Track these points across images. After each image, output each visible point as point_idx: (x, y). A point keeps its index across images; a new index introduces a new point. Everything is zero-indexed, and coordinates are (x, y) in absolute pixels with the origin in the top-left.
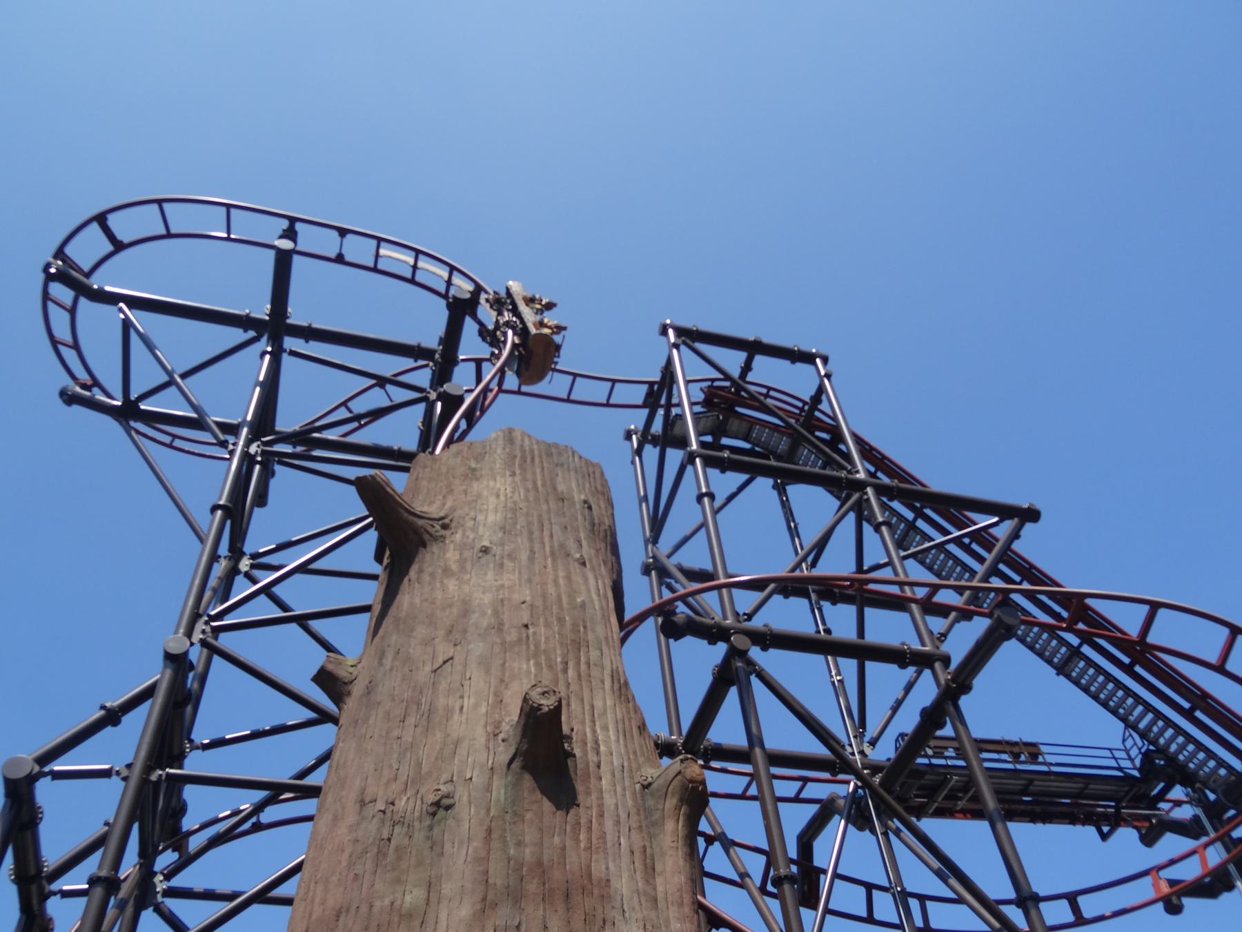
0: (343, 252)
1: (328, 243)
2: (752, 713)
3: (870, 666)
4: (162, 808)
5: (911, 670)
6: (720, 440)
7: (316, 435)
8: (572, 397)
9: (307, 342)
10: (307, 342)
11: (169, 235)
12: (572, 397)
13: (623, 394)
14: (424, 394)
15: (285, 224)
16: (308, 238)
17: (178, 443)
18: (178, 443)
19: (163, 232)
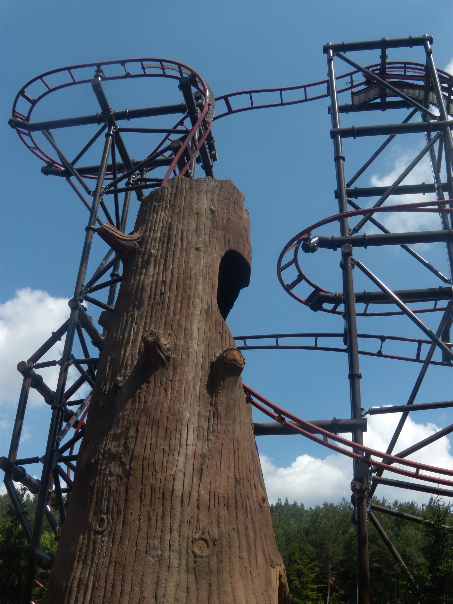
0: (123, 67)
1: (119, 70)
2: (124, 225)
3: (246, 340)
4: (209, 95)
5: (345, 347)
6: (385, 100)
7: (160, 157)
8: (308, 98)
9: (366, 247)
10: (366, 247)
11: (50, 91)
12: (303, 89)
13: (312, 92)
14: (349, 199)
15: (95, 68)
16: (108, 71)
17: (413, 470)
18: (413, 470)
19: (48, 90)
